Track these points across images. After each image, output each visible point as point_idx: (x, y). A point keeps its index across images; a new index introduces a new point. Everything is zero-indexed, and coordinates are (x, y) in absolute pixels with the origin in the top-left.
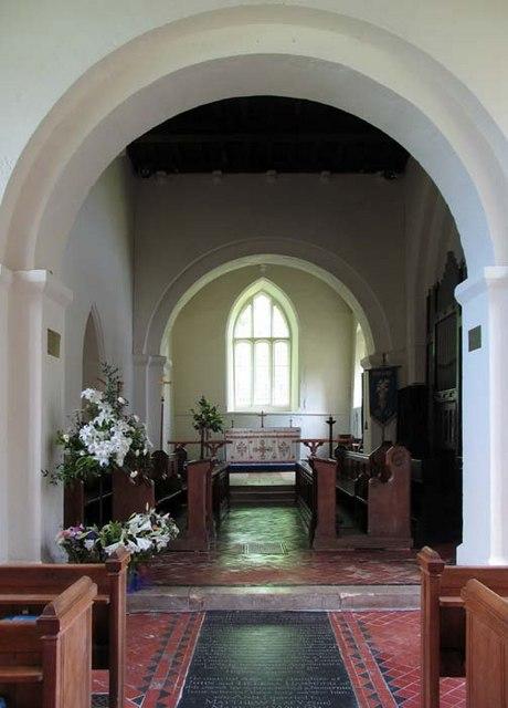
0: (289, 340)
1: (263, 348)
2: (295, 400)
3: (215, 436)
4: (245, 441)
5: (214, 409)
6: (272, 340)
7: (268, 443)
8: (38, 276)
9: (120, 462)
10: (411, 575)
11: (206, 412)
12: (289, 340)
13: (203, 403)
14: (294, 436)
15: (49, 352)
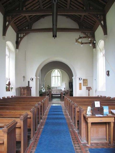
0: (60, 76)
1: (56, 77)
2: (61, 85)
3: (50, 90)
4: (54, 91)
6: (58, 76)
8: (38, 77)
11: (49, 87)
12: (60, 76)
13: (48, 86)
14: (61, 90)
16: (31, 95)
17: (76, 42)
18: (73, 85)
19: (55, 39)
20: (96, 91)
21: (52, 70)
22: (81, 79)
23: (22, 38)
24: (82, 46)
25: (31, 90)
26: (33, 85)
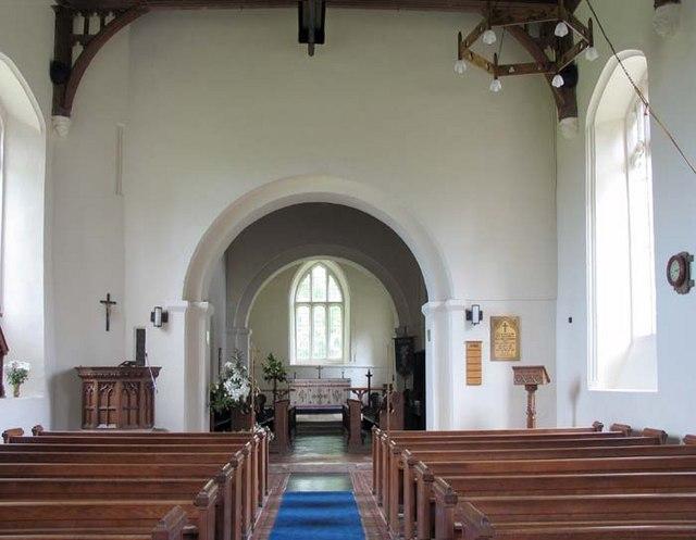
0: (342, 304)
1: (319, 311)
2: (347, 356)
3: (281, 385)
4: (305, 389)
5: (280, 363)
6: (327, 304)
7: (325, 391)
8: (204, 305)
9: (245, 400)
10: (437, 492)
12: (342, 304)
13: (271, 358)
14: (346, 385)
15: (144, 330)
16: (151, 419)
17: (460, 59)
18: (422, 355)
19: (311, 53)
20: (575, 392)
21: (297, 262)
22: (481, 314)
23: (92, 44)
24: (497, 86)
25: (150, 391)
26: (170, 355)
